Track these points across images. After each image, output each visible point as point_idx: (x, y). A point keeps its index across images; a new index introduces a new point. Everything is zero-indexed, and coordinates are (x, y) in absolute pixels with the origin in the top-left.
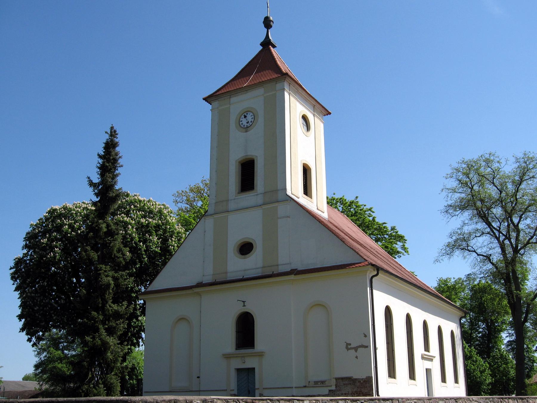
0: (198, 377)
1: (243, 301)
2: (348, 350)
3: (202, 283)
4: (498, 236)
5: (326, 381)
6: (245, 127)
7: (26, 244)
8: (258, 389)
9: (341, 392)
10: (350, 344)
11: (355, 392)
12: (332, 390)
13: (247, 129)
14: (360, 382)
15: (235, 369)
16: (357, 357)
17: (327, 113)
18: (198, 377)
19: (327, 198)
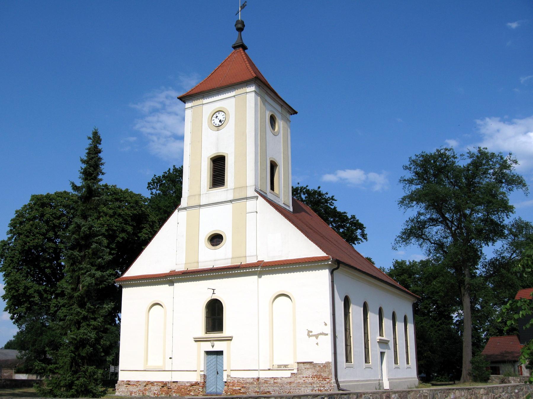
0: (170, 358)
1: (213, 289)
2: (309, 337)
3: (175, 271)
4: (450, 226)
5: (288, 365)
6: (217, 125)
7: (11, 230)
8: (226, 370)
9: (302, 375)
10: (311, 332)
11: (315, 376)
12: (294, 373)
13: (218, 127)
14: (320, 366)
15: (205, 351)
16: (317, 344)
17: (294, 112)
18: (170, 358)
19: (292, 187)
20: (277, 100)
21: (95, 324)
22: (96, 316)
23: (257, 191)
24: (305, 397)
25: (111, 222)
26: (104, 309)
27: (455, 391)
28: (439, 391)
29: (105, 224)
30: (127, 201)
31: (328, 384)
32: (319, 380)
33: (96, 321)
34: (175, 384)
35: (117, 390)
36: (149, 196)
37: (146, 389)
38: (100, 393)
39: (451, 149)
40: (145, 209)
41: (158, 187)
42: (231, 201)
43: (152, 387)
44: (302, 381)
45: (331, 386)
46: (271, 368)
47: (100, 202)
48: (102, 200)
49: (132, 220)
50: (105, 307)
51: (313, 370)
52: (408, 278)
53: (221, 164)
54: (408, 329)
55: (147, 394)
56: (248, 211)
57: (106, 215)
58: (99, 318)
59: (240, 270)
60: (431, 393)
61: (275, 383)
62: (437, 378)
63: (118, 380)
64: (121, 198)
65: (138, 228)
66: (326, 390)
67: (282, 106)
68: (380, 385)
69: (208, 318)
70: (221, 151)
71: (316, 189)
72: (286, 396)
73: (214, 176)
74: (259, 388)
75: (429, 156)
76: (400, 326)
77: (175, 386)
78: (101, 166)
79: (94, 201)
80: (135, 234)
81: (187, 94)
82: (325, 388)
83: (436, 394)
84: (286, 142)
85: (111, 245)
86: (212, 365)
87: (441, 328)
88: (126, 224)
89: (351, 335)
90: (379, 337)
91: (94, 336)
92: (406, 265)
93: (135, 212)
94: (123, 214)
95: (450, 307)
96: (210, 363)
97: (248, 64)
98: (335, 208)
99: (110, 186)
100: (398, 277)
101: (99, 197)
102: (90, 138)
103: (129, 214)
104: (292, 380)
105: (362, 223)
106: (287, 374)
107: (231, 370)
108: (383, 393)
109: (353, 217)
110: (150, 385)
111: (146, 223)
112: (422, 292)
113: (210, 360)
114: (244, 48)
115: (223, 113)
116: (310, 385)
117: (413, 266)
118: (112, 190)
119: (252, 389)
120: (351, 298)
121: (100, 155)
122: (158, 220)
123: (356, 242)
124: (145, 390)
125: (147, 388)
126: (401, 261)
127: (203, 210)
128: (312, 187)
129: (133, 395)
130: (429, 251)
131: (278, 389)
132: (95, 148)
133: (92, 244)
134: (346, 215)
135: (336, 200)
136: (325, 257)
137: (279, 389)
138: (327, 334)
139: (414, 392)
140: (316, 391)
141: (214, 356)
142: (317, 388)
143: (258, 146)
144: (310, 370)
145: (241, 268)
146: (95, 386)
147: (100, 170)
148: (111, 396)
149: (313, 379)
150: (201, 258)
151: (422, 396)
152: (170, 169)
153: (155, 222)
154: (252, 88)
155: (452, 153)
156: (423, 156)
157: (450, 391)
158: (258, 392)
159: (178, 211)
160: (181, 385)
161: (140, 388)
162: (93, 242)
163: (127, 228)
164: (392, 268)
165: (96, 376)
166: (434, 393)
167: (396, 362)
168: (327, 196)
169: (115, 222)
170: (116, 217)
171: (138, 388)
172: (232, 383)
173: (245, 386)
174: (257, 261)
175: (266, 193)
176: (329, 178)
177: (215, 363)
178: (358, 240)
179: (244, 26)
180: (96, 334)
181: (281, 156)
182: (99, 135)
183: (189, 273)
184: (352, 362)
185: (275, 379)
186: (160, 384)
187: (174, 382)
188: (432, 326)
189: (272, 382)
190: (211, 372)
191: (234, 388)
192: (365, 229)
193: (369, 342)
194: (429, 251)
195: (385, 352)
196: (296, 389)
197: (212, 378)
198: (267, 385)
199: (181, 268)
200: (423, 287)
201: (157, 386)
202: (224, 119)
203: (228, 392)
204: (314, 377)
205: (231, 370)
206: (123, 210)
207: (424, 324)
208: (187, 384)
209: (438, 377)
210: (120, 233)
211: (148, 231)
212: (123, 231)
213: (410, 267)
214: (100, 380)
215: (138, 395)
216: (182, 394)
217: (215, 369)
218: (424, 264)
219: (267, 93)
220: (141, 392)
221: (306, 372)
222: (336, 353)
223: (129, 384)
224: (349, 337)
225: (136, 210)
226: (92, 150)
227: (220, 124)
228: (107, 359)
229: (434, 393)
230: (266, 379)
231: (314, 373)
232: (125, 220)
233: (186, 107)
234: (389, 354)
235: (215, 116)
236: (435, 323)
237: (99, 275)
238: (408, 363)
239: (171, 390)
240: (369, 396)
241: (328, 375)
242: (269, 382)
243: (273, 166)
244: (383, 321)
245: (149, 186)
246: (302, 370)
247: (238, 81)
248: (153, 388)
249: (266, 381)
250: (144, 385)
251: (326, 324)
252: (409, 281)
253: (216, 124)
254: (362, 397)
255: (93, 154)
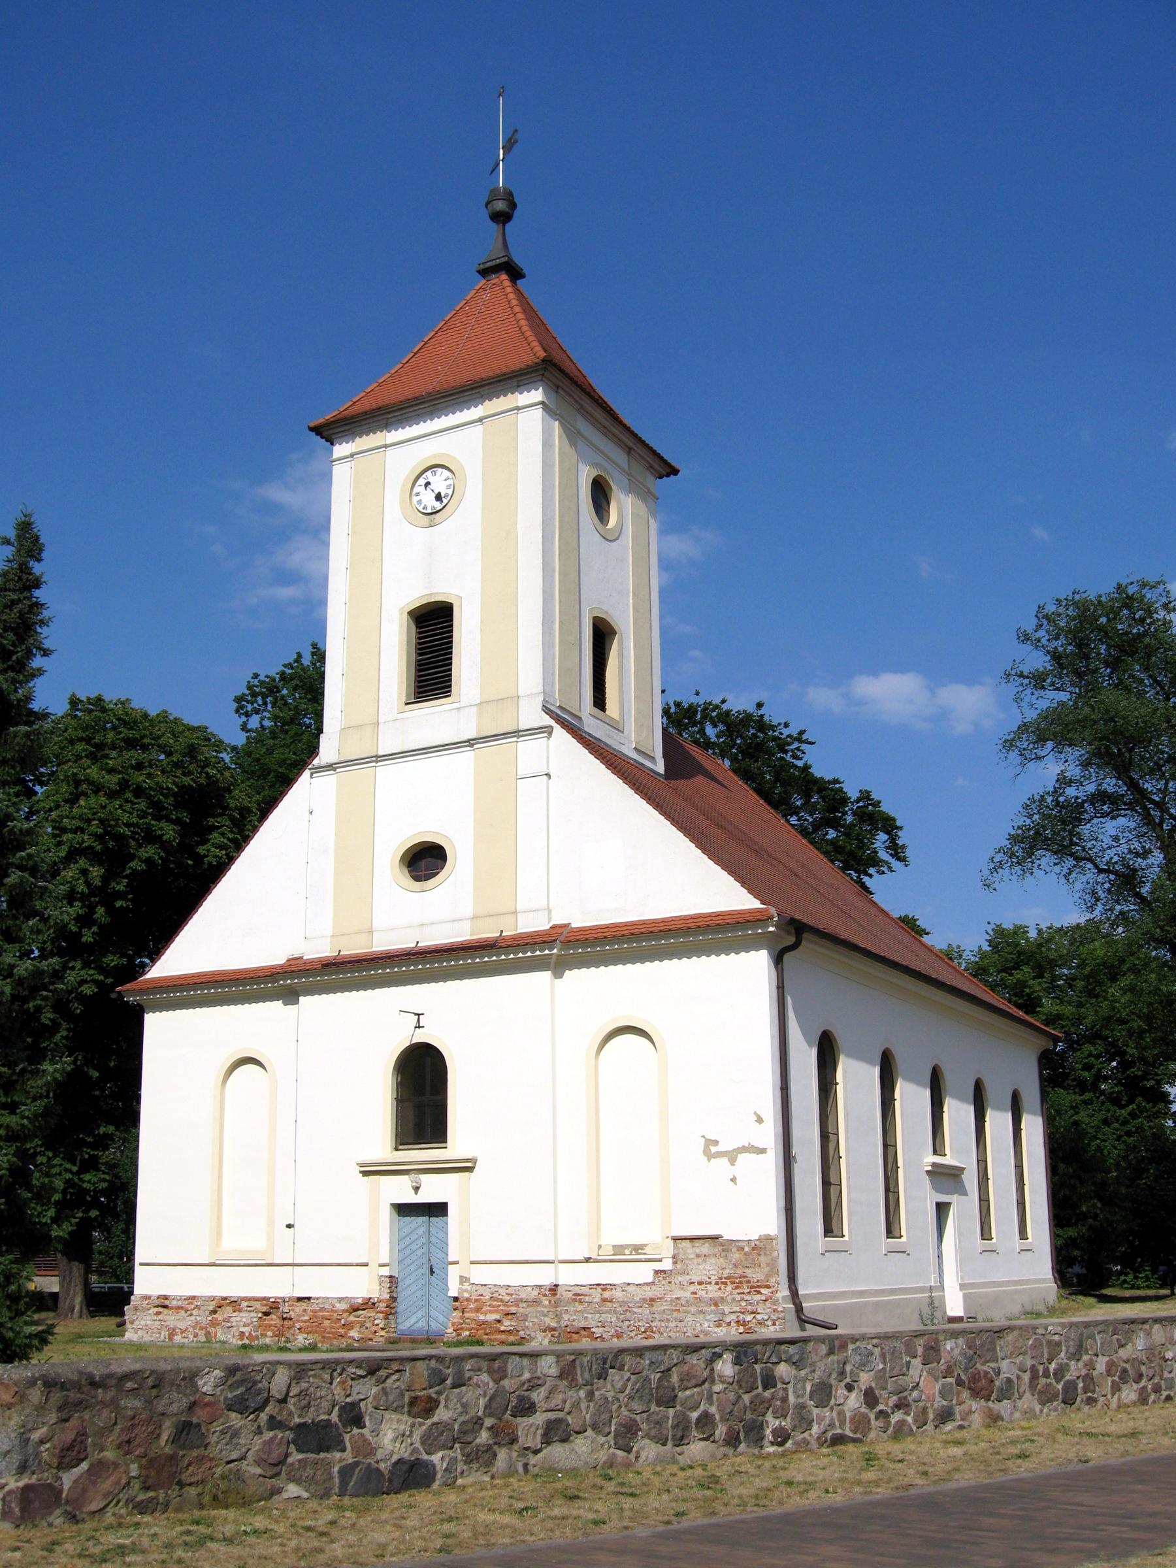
0: (289, 1226)
1: (416, 1014)
6: (429, 511)
8: (457, 1263)
9: (688, 1278)
10: (716, 1143)
12: (664, 1272)
14: (743, 1249)
15: (393, 1205)
16: (734, 1180)
17: (668, 470)
18: (289, 1226)
20: (612, 429)
21: (13, 1125)
22: (16, 1098)
23: (552, 711)
24: (658, 1352)
25: (111, 813)
26: (43, 1076)
27: (1151, 1328)
28: (1099, 1328)
29: (94, 819)
30: (162, 748)
31: (767, 1303)
32: (739, 1291)
33: (15, 1114)
34: (304, 1305)
35: (128, 1325)
36: (239, 739)
37: (216, 1319)
38: (28, 1341)
39: (1159, 583)
40: (218, 771)
41: (269, 706)
42: (470, 743)
43: (235, 1314)
44: (688, 1295)
45: (775, 1310)
46: (594, 1256)
47: (31, 740)
48: (39, 733)
49: (177, 806)
50: (44, 1071)
51: (721, 1260)
52: (1034, 978)
53: (441, 628)
54: (1023, 1133)
55: (218, 1335)
56: (521, 773)
57: (97, 789)
58: (26, 1105)
59: (498, 955)
60: (1073, 1336)
61: (605, 1300)
62: (1122, 1278)
63: (131, 1293)
64: (143, 737)
65: (196, 831)
66: (760, 1324)
67: (630, 449)
68: (935, 1304)
69: (401, 1101)
70: (440, 591)
71: (751, 708)
72: (595, 1349)
73: (420, 665)
74: (558, 1316)
75: (1093, 604)
76: (998, 1122)
77: (305, 1310)
78: (39, 630)
79: (15, 737)
80: (187, 848)
81: (339, 417)
82: (759, 1317)
83: (1088, 1337)
84: (641, 560)
85: (113, 884)
86: (414, 1247)
87: (1133, 1129)
88: (158, 818)
89: (842, 1153)
90: (932, 1159)
91: (8, 1161)
92: (1027, 940)
93: (187, 780)
94: (150, 788)
95: (1161, 1065)
96: (407, 1241)
97: (523, 322)
98: (806, 767)
99: (111, 701)
100: (1004, 974)
101: (29, 723)
102: (7, 542)
103: (168, 788)
104: (655, 1292)
105: (892, 813)
106: (642, 1273)
107: (472, 1263)
108: (916, 1336)
109: (865, 796)
110: (229, 1309)
111: (221, 815)
112: (1078, 1019)
113: (407, 1230)
114: (515, 274)
115: (446, 473)
116: (713, 1308)
117: (1049, 940)
118: (115, 715)
119: (536, 1320)
120: (842, 1038)
121: (37, 593)
122: (259, 804)
123: (872, 871)
124: (214, 1323)
125: (220, 1318)
126: (1011, 927)
127: (385, 771)
128: (739, 703)
129: (178, 1339)
130: (1094, 893)
131: (614, 1320)
132: (21, 571)
133: (6, 870)
134: (841, 789)
135: (814, 743)
136: (758, 910)
137: (618, 1318)
138: (762, 1151)
139: (1015, 1333)
140: (729, 1324)
141: (421, 1220)
142: (733, 1317)
143: (554, 571)
144: (713, 1260)
145: (501, 947)
146: (11, 1318)
147: (35, 640)
148: (109, 1343)
149: (720, 1289)
150: (380, 920)
151: (1041, 1345)
152: (299, 655)
153: (248, 810)
154: (536, 395)
155: (1164, 594)
156: (1076, 604)
157: (1133, 1327)
158: (554, 1329)
159: (312, 774)
160: (322, 1310)
161: (198, 1318)
162: (12, 865)
163: (161, 829)
164: (986, 947)
165: (13, 1287)
166: (1082, 1334)
167: (985, 1233)
168: (786, 732)
169: (124, 811)
170: (129, 795)
171: (192, 1318)
172: (476, 1300)
173: (513, 1309)
174: (551, 925)
175: (580, 718)
176: (822, 698)
177: (424, 1240)
178: (878, 865)
179: (513, 205)
180: (14, 1155)
181: (628, 605)
182: (35, 530)
183: (342, 963)
184: (843, 1236)
185: (605, 1287)
186: (258, 1305)
187: (300, 1299)
188: (1106, 1122)
189: (597, 1300)
190: (412, 1268)
191: (482, 1317)
192: (900, 833)
193: (901, 1172)
194: (1094, 893)
195: (950, 1204)
196: (668, 1320)
197: (413, 1288)
198: (580, 1308)
199: (318, 949)
200: (1080, 1005)
201: (250, 1311)
202: (450, 492)
203: (461, 1329)
204: (725, 1284)
205: (472, 1263)
206: (149, 776)
207: (1082, 1116)
208: (338, 1305)
209: (1126, 1274)
210: (140, 846)
211: (228, 839)
212: (151, 837)
213: (1040, 945)
214: (27, 1299)
215: (191, 1337)
216: (323, 1337)
217: (425, 1260)
218: (1081, 935)
219: (582, 410)
220: (201, 1328)
221: (701, 1267)
222: (791, 1209)
223: (165, 1307)
224: (836, 1157)
225: (190, 773)
226: (12, 580)
227: (438, 506)
228: (54, 1234)
229: (1082, 1334)
230: (577, 1290)
231: (723, 1269)
232: (157, 806)
233: (335, 456)
234: (963, 1208)
235: (422, 481)
236: (1115, 1112)
237: (26, 970)
238: (1023, 1235)
239: (291, 1322)
240: (870, 1347)
241: (768, 1276)
242: (587, 1299)
243: (602, 635)
244: (945, 1109)
245: (242, 707)
246: (687, 1262)
247: (491, 374)
248: (238, 1319)
249: (579, 1295)
250: (211, 1308)
251: (760, 1120)
252: (1037, 986)
253: (425, 508)
254: (847, 1351)
255: (15, 591)
